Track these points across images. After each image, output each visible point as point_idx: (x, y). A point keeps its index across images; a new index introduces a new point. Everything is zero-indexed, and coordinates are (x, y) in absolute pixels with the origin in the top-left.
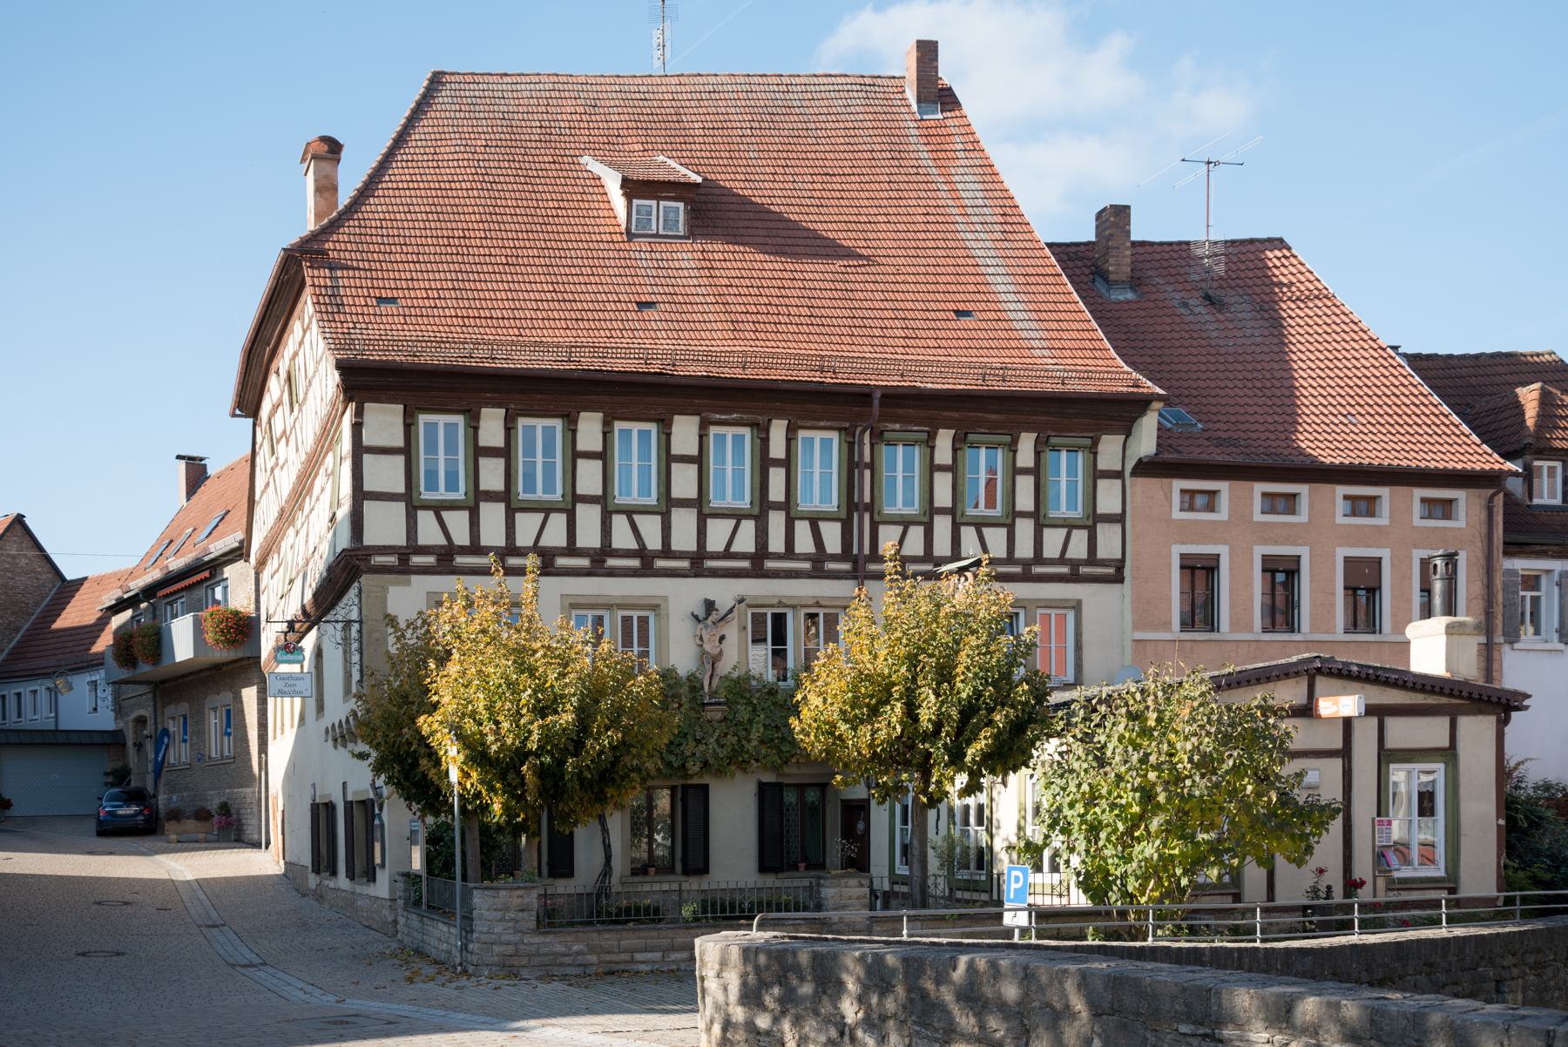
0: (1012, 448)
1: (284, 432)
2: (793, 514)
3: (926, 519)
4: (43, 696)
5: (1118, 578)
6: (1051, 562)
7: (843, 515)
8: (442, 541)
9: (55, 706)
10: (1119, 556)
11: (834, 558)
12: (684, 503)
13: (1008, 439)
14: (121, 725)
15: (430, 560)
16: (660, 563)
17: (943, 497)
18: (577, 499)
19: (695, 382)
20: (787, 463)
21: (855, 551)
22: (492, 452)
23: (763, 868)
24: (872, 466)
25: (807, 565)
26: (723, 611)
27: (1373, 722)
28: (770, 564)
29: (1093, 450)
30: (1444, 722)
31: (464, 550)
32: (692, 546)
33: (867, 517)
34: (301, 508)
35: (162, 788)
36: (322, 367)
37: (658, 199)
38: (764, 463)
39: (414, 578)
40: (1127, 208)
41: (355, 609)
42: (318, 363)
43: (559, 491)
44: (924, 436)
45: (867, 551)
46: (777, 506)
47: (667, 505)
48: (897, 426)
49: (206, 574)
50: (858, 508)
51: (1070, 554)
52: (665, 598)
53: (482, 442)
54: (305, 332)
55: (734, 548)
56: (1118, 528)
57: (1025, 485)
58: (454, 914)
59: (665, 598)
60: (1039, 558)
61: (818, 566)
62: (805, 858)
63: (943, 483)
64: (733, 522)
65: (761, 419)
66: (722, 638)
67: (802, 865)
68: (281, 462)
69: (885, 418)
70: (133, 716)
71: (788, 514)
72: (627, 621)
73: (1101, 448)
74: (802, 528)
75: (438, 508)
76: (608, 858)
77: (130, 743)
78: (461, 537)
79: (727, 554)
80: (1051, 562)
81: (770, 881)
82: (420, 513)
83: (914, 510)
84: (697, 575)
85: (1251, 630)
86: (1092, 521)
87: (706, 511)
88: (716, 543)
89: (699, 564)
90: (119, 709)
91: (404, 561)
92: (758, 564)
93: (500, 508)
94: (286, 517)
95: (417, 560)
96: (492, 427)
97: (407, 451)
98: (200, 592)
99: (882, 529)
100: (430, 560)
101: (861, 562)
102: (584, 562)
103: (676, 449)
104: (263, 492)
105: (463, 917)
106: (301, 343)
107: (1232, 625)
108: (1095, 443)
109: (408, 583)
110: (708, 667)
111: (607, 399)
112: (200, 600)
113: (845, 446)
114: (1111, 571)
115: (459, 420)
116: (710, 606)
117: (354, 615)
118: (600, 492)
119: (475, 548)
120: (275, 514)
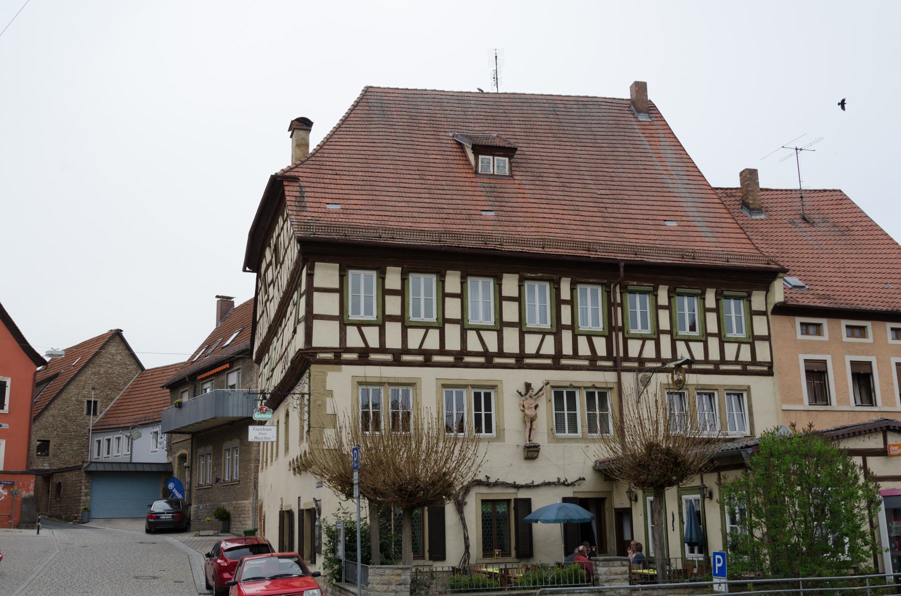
2: (576, 332)
3: (655, 337)
4: (124, 441)
5: (770, 373)
7: (606, 334)
8: (362, 345)
10: (769, 360)
11: (602, 358)
12: (511, 325)
13: (699, 291)
14: (171, 459)
15: (354, 356)
16: (497, 360)
18: (446, 321)
20: (572, 302)
21: (615, 355)
22: (393, 292)
24: (621, 305)
25: (586, 363)
26: (536, 391)
28: (564, 362)
31: (375, 351)
32: (516, 350)
33: (620, 335)
37: (494, 155)
38: (558, 302)
39: (344, 367)
41: (307, 386)
42: (290, 239)
43: (435, 317)
44: (651, 289)
45: (621, 354)
47: (500, 326)
48: (635, 283)
49: (227, 366)
50: (613, 330)
51: (426, 346)
52: (501, 381)
53: (387, 287)
56: (767, 344)
57: (712, 318)
59: (501, 381)
61: (593, 364)
63: (664, 316)
66: (536, 407)
68: (270, 297)
72: (477, 396)
73: (753, 298)
74: (582, 341)
75: (360, 325)
76: (467, 547)
78: (374, 343)
79: (538, 355)
84: (520, 368)
86: (752, 340)
88: (531, 348)
89: (520, 361)
92: (556, 362)
93: (398, 325)
94: (273, 331)
95: (346, 356)
96: (393, 279)
97: (341, 291)
98: (224, 377)
99: (630, 342)
100: (354, 356)
101: (618, 361)
102: (451, 359)
103: (505, 293)
104: (261, 316)
106: (282, 228)
107: (838, 401)
108: (749, 295)
109: (340, 370)
110: (529, 424)
112: (223, 382)
113: (605, 294)
114: (766, 369)
116: (528, 386)
117: (306, 390)
118: (459, 317)
120: (267, 326)
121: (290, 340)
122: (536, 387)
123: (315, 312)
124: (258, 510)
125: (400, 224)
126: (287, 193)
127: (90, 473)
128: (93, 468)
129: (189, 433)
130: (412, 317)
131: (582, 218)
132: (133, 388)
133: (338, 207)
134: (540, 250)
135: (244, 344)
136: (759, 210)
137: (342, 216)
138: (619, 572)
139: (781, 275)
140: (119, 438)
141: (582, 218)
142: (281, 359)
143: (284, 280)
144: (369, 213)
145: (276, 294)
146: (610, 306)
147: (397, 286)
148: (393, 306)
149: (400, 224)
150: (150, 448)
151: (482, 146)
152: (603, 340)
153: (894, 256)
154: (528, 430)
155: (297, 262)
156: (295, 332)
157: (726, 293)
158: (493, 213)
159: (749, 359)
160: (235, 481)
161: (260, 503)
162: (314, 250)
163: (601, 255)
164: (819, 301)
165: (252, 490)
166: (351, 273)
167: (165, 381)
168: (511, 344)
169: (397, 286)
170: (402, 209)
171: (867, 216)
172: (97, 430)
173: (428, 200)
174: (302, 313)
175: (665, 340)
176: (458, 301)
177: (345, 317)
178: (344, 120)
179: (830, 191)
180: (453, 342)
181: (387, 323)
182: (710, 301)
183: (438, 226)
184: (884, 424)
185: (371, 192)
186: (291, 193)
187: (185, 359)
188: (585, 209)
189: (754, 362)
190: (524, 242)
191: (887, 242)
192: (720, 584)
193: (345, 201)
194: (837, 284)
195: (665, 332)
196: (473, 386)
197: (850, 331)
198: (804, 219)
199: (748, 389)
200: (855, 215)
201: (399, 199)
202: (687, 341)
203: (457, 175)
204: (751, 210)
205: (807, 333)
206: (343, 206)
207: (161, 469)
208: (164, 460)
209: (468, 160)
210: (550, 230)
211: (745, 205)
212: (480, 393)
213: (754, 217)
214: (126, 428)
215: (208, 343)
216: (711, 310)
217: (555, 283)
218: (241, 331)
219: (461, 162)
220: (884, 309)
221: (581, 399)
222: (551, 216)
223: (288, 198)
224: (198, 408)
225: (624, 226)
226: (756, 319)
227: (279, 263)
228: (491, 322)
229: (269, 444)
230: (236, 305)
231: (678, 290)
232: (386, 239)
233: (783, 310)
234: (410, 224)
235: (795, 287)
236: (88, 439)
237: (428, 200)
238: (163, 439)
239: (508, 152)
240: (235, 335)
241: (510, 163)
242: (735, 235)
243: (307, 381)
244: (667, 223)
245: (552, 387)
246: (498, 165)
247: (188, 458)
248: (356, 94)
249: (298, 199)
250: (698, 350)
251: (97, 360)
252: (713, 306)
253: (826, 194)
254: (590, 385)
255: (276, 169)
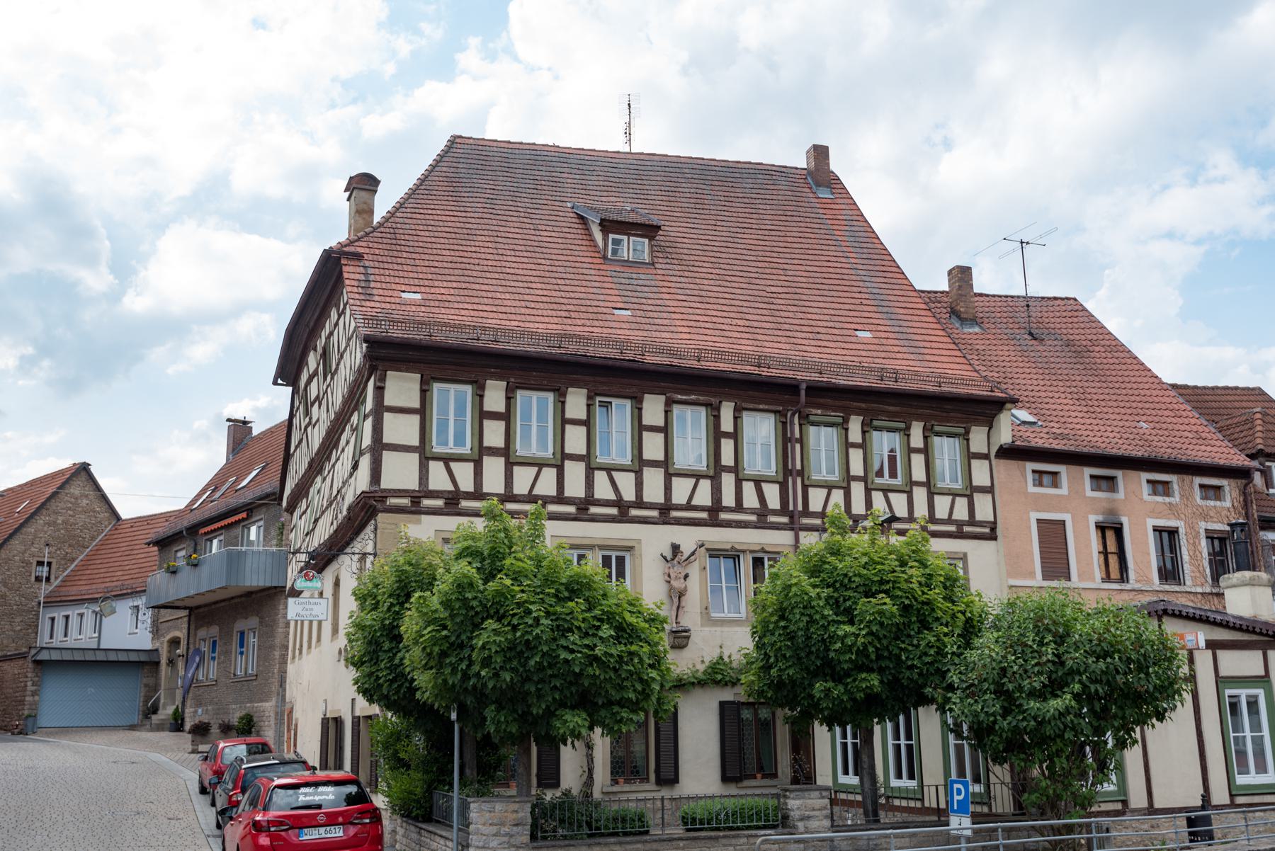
0: (906, 432)
1: (318, 397)
2: (741, 476)
3: (845, 485)
4: (89, 620)
5: (992, 536)
6: (942, 522)
7: (781, 479)
8: (450, 487)
9: (98, 628)
10: (992, 519)
11: (775, 513)
12: (654, 464)
13: (903, 425)
14: (157, 645)
15: (439, 503)
16: (634, 512)
17: (857, 468)
18: (565, 456)
19: (661, 369)
20: (735, 436)
21: (791, 508)
22: (494, 416)
23: (726, 779)
24: (801, 441)
25: (753, 518)
26: (686, 555)
27: (1209, 652)
28: (724, 516)
29: (965, 436)
30: (1258, 655)
31: (468, 496)
32: (660, 499)
33: (799, 480)
34: (329, 458)
35: (189, 703)
36: (352, 343)
37: (629, 235)
38: (716, 436)
39: (423, 517)
40: (969, 269)
41: (371, 544)
42: (349, 339)
43: (551, 450)
44: (840, 420)
45: (800, 508)
46: (728, 469)
47: (639, 465)
48: (819, 412)
49: (244, 515)
50: (790, 473)
51: (539, 490)
53: (487, 407)
54: (339, 316)
55: (695, 502)
56: (989, 497)
57: (918, 461)
58: (452, 827)
60: (932, 519)
61: (762, 519)
62: (761, 769)
63: (856, 457)
64: (694, 480)
65: (714, 400)
66: (686, 577)
67: (759, 776)
68: (314, 420)
69: (809, 404)
70: (168, 637)
71: (737, 476)
73: (971, 436)
74: (749, 488)
75: (447, 460)
76: (591, 770)
77: (164, 661)
78: (467, 484)
79: (689, 507)
80: (942, 522)
81: (732, 789)
82: (431, 463)
83: (835, 477)
84: (665, 523)
85: (1093, 580)
86: (970, 491)
87: (671, 471)
88: (679, 497)
89: (665, 513)
90: (156, 631)
91: (415, 503)
92: (713, 515)
94: (317, 466)
95: (427, 502)
96: (495, 397)
97: (423, 411)
98: (238, 531)
99: (811, 491)
100: (439, 503)
101: (796, 517)
102: (571, 509)
103: (647, 421)
104: (297, 447)
105: (459, 830)
106: (337, 324)
107: (1079, 576)
108: (967, 432)
109: (419, 522)
110: (676, 600)
111: (591, 379)
112: (236, 537)
113: (780, 425)
114: (987, 530)
115: (468, 390)
116: (676, 549)
117: (370, 549)
118: (584, 452)
119: (478, 494)
120: (306, 461)
121: (347, 479)
122: (686, 549)
123: (385, 441)
124: (285, 716)
125: (503, 322)
126: (346, 275)
127: (38, 663)
128: (44, 656)
129: (185, 608)
130: (520, 450)
131: (747, 323)
132: (103, 543)
133: (418, 296)
134: (694, 364)
135: (270, 485)
136: (974, 321)
137: (423, 309)
138: (817, 807)
139: (1008, 406)
140: (81, 615)
141: (747, 323)
142: (330, 504)
143: (337, 396)
144: (461, 306)
145: (324, 415)
146: (786, 441)
147: (500, 407)
148: (494, 434)
149: (503, 322)
150: (127, 629)
151: (617, 222)
152: (776, 487)
153: (1147, 386)
154: (675, 608)
155: (360, 371)
156: (355, 467)
157: (937, 428)
158: (629, 313)
159: (965, 517)
160: (251, 675)
161: (288, 707)
162: (385, 354)
163: (775, 372)
164: (1057, 442)
165: (275, 687)
166: (437, 387)
167: (152, 536)
168: (654, 489)
169: (500, 407)
170: (506, 303)
171: (1110, 333)
172: (51, 602)
173: (541, 292)
174: (367, 441)
175: (857, 490)
176: (583, 429)
177: (427, 448)
178: (423, 180)
179: (1062, 299)
180: (575, 487)
181: (485, 458)
182: (917, 440)
183: (555, 327)
184: (1161, 607)
185: (462, 279)
186: (352, 276)
187: (181, 504)
188: (751, 311)
189: (972, 521)
190: (671, 352)
191: (1136, 367)
192: (960, 824)
193: (427, 290)
194: (1076, 420)
195: (857, 478)
196: (602, 547)
197: (1095, 481)
198: (1031, 334)
199: (964, 558)
200: (1094, 331)
201: (501, 289)
202: (886, 491)
203: (579, 259)
204: (963, 320)
205: (1041, 484)
206: (425, 296)
207: (143, 658)
208: (149, 646)
209: (593, 240)
210: (706, 338)
211: (954, 312)
212: (610, 557)
213: (966, 330)
214: (94, 600)
215: (215, 484)
216: (917, 451)
217: (713, 409)
218: (263, 468)
219: (584, 243)
220: (1140, 454)
221: (746, 564)
222: (706, 319)
223: (347, 282)
224: (211, 568)
225: (803, 335)
226: (975, 463)
227: (329, 371)
228: (627, 460)
229: (306, 624)
230: (255, 432)
231: (876, 423)
232: (486, 342)
233: (1011, 453)
234: (516, 323)
235: (1024, 423)
236: (37, 615)
237: (541, 292)
238: (147, 617)
239: (649, 230)
240: (254, 473)
241: (651, 246)
242: (948, 353)
243: (372, 536)
244: (858, 333)
245: (708, 550)
246: (633, 248)
247: (183, 643)
248: (441, 145)
249: (363, 284)
250: (899, 504)
251: (53, 505)
252: (920, 445)
253: (1058, 302)
254: (757, 548)
255: (332, 243)
